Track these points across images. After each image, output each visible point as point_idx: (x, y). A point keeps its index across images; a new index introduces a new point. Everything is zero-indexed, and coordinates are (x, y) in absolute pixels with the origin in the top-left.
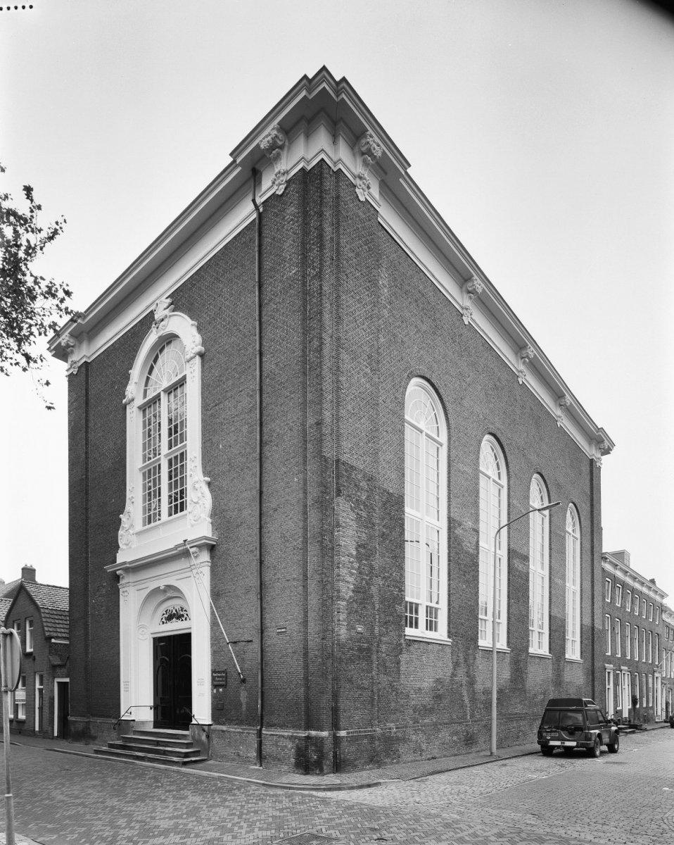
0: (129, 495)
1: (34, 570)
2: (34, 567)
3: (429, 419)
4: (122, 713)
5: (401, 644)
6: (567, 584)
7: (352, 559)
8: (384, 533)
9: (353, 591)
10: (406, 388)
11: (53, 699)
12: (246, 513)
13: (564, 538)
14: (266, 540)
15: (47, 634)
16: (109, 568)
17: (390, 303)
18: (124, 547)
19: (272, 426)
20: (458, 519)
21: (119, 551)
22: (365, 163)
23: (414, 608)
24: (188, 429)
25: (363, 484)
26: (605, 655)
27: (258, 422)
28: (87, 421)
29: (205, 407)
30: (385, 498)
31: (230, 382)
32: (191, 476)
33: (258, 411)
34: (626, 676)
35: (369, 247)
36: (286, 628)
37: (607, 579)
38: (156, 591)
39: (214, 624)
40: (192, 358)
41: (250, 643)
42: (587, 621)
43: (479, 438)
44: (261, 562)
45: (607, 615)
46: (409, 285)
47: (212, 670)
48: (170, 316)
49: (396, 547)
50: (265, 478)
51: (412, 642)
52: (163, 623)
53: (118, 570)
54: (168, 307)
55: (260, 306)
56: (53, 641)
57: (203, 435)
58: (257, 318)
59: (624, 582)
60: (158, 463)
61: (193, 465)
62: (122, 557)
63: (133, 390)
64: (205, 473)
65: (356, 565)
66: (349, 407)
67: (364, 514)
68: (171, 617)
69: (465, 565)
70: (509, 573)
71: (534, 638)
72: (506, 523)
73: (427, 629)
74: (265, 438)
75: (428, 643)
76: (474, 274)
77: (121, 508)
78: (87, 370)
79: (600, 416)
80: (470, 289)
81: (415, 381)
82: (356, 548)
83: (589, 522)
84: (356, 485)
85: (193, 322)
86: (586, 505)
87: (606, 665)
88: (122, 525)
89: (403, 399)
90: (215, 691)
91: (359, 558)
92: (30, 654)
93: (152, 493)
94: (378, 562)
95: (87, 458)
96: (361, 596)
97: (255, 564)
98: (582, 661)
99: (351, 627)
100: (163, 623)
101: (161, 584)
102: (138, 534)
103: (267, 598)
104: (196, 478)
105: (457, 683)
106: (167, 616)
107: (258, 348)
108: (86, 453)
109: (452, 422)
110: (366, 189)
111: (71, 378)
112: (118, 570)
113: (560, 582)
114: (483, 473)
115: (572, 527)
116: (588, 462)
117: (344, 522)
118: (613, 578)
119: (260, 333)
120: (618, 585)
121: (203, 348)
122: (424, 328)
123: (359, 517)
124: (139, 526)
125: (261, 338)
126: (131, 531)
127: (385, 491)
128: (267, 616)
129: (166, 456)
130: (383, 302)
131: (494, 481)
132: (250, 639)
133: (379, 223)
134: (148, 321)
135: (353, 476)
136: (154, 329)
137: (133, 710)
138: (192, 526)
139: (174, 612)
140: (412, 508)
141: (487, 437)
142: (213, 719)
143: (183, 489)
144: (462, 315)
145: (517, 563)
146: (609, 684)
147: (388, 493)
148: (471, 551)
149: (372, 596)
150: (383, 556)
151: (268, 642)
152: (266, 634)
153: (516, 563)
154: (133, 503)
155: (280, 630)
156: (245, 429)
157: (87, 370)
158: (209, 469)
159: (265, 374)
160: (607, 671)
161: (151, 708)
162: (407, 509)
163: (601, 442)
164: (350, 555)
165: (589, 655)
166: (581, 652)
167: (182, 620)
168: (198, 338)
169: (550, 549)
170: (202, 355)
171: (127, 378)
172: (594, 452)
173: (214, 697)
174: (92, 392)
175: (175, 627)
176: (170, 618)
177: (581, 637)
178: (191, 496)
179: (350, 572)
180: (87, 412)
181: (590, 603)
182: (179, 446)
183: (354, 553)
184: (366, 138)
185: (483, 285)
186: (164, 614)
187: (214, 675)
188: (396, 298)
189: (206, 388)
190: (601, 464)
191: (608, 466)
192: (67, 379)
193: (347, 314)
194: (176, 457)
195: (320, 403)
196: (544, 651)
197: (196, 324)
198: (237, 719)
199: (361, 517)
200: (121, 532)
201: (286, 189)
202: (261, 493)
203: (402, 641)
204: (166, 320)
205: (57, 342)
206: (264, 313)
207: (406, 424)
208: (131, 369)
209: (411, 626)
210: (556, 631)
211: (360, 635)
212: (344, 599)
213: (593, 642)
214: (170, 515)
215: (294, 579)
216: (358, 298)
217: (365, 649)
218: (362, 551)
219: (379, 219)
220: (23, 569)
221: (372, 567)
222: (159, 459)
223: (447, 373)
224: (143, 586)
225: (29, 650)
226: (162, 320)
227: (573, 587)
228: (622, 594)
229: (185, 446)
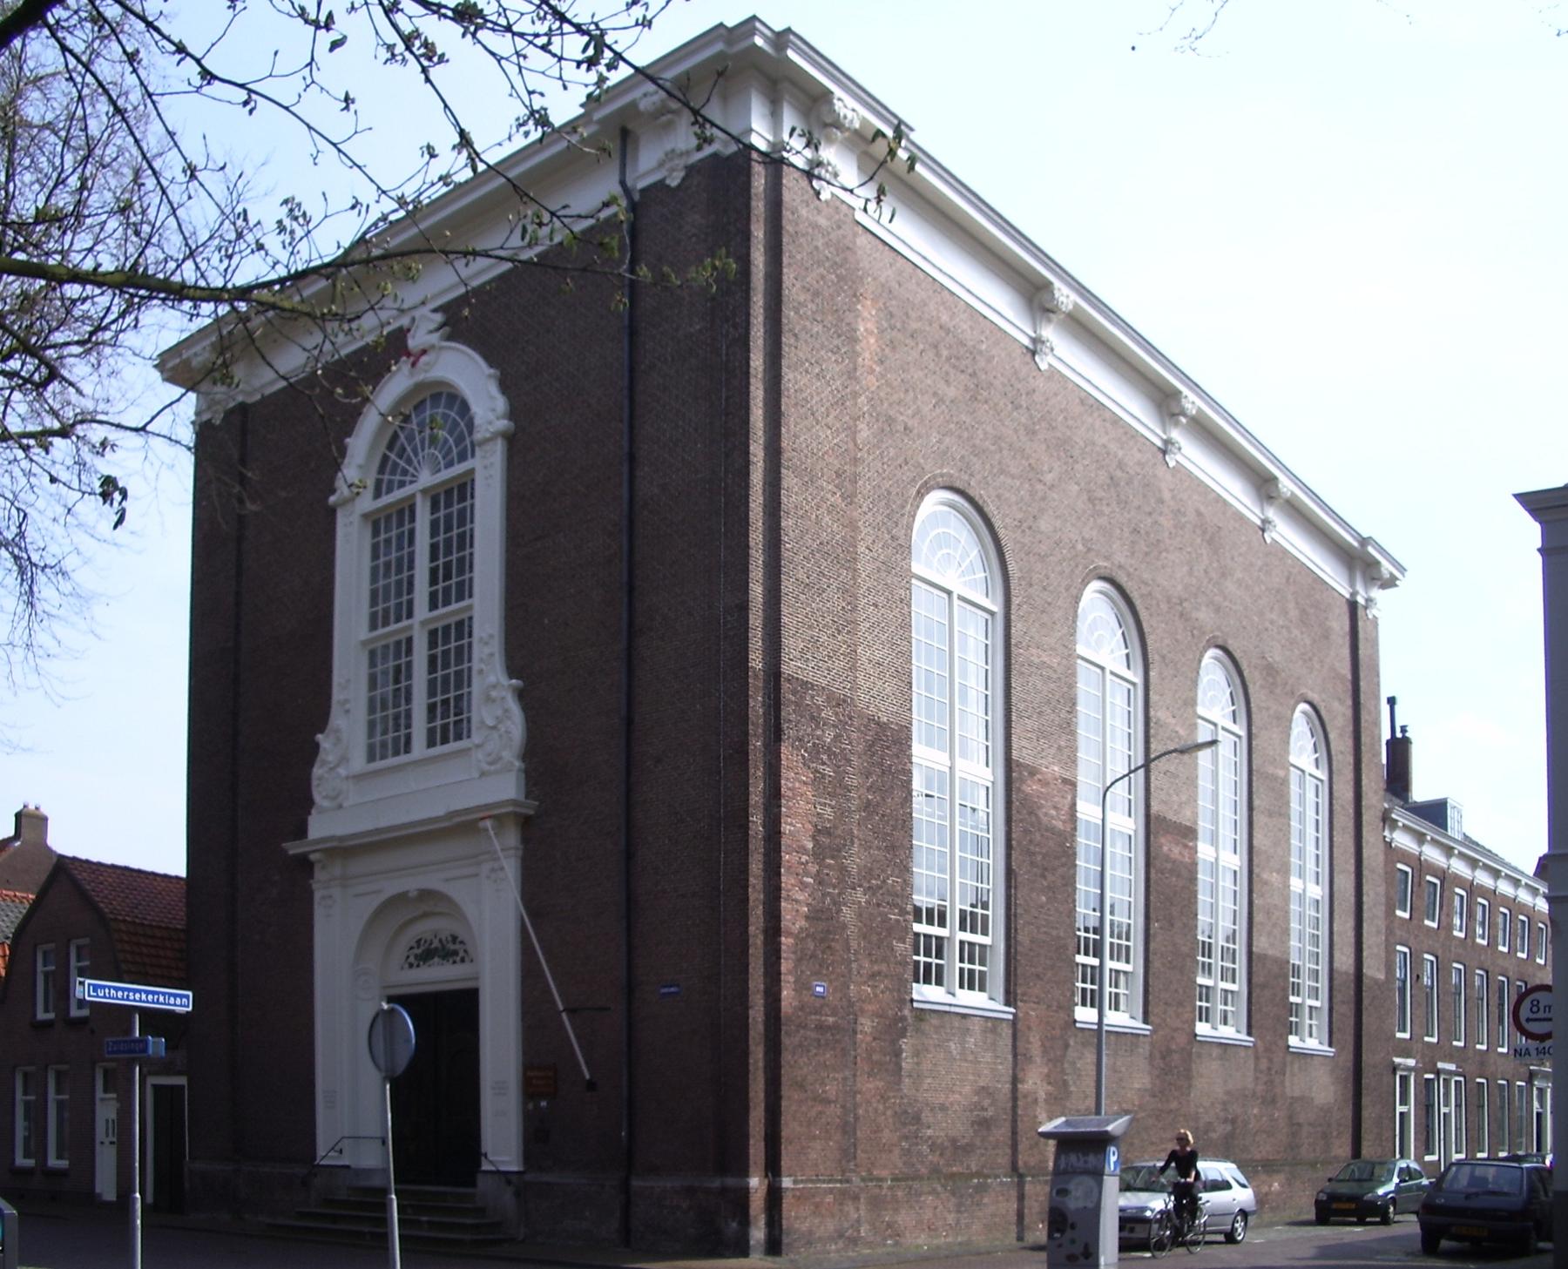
0: (337, 695)
2: (44, 810)
3: (964, 565)
4: (321, 1152)
5: (903, 1019)
7: (804, 858)
8: (869, 802)
9: (807, 918)
10: (914, 517)
13: (1285, 782)
16: (294, 848)
18: (326, 803)
21: (313, 811)
24: (477, 574)
36: (678, 986)
37: (1400, 866)
38: (400, 900)
42: (1345, 961)
43: (1074, 592)
46: (920, 319)
51: (921, 1015)
53: (314, 851)
61: (487, 650)
62: (320, 827)
64: (512, 671)
65: (813, 868)
66: (801, 575)
67: (828, 771)
68: (427, 953)
69: (1045, 856)
73: (961, 986)
75: (964, 1016)
77: (320, 718)
82: (814, 838)
83: (1350, 742)
85: (492, 371)
87: (1397, 1060)
88: (322, 756)
89: (909, 537)
90: (531, 1106)
94: (855, 859)
99: (803, 986)
100: (411, 966)
102: (359, 778)
104: (492, 679)
106: (418, 951)
111: (204, 431)
112: (314, 851)
113: (1274, 878)
117: (789, 789)
118: (1416, 864)
120: (1429, 878)
121: (512, 424)
122: (951, 392)
123: (819, 778)
124: (358, 762)
127: (871, 719)
129: (423, 623)
134: (395, 346)
137: (345, 1144)
138: (483, 774)
140: (929, 743)
145: (1168, 847)
146: (1404, 1101)
147: (878, 724)
148: (1060, 825)
150: (866, 846)
154: (347, 711)
160: (1399, 1074)
167: (454, 962)
168: (501, 403)
175: (438, 976)
178: (481, 713)
183: (810, 845)
186: (412, 948)
187: (529, 1074)
188: (894, 349)
193: (796, 404)
194: (447, 628)
197: (498, 373)
199: (824, 776)
200: (317, 771)
201: (684, 179)
202: (629, 722)
203: (906, 1012)
208: (349, 434)
210: (1264, 986)
211: (822, 1001)
212: (789, 934)
216: (817, 371)
217: (829, 1027)
218: (825, 840)
220: (18, 816)
221: (843, 869)
223: (1002, 472)
226: (424, 352)
229: (470, 607)
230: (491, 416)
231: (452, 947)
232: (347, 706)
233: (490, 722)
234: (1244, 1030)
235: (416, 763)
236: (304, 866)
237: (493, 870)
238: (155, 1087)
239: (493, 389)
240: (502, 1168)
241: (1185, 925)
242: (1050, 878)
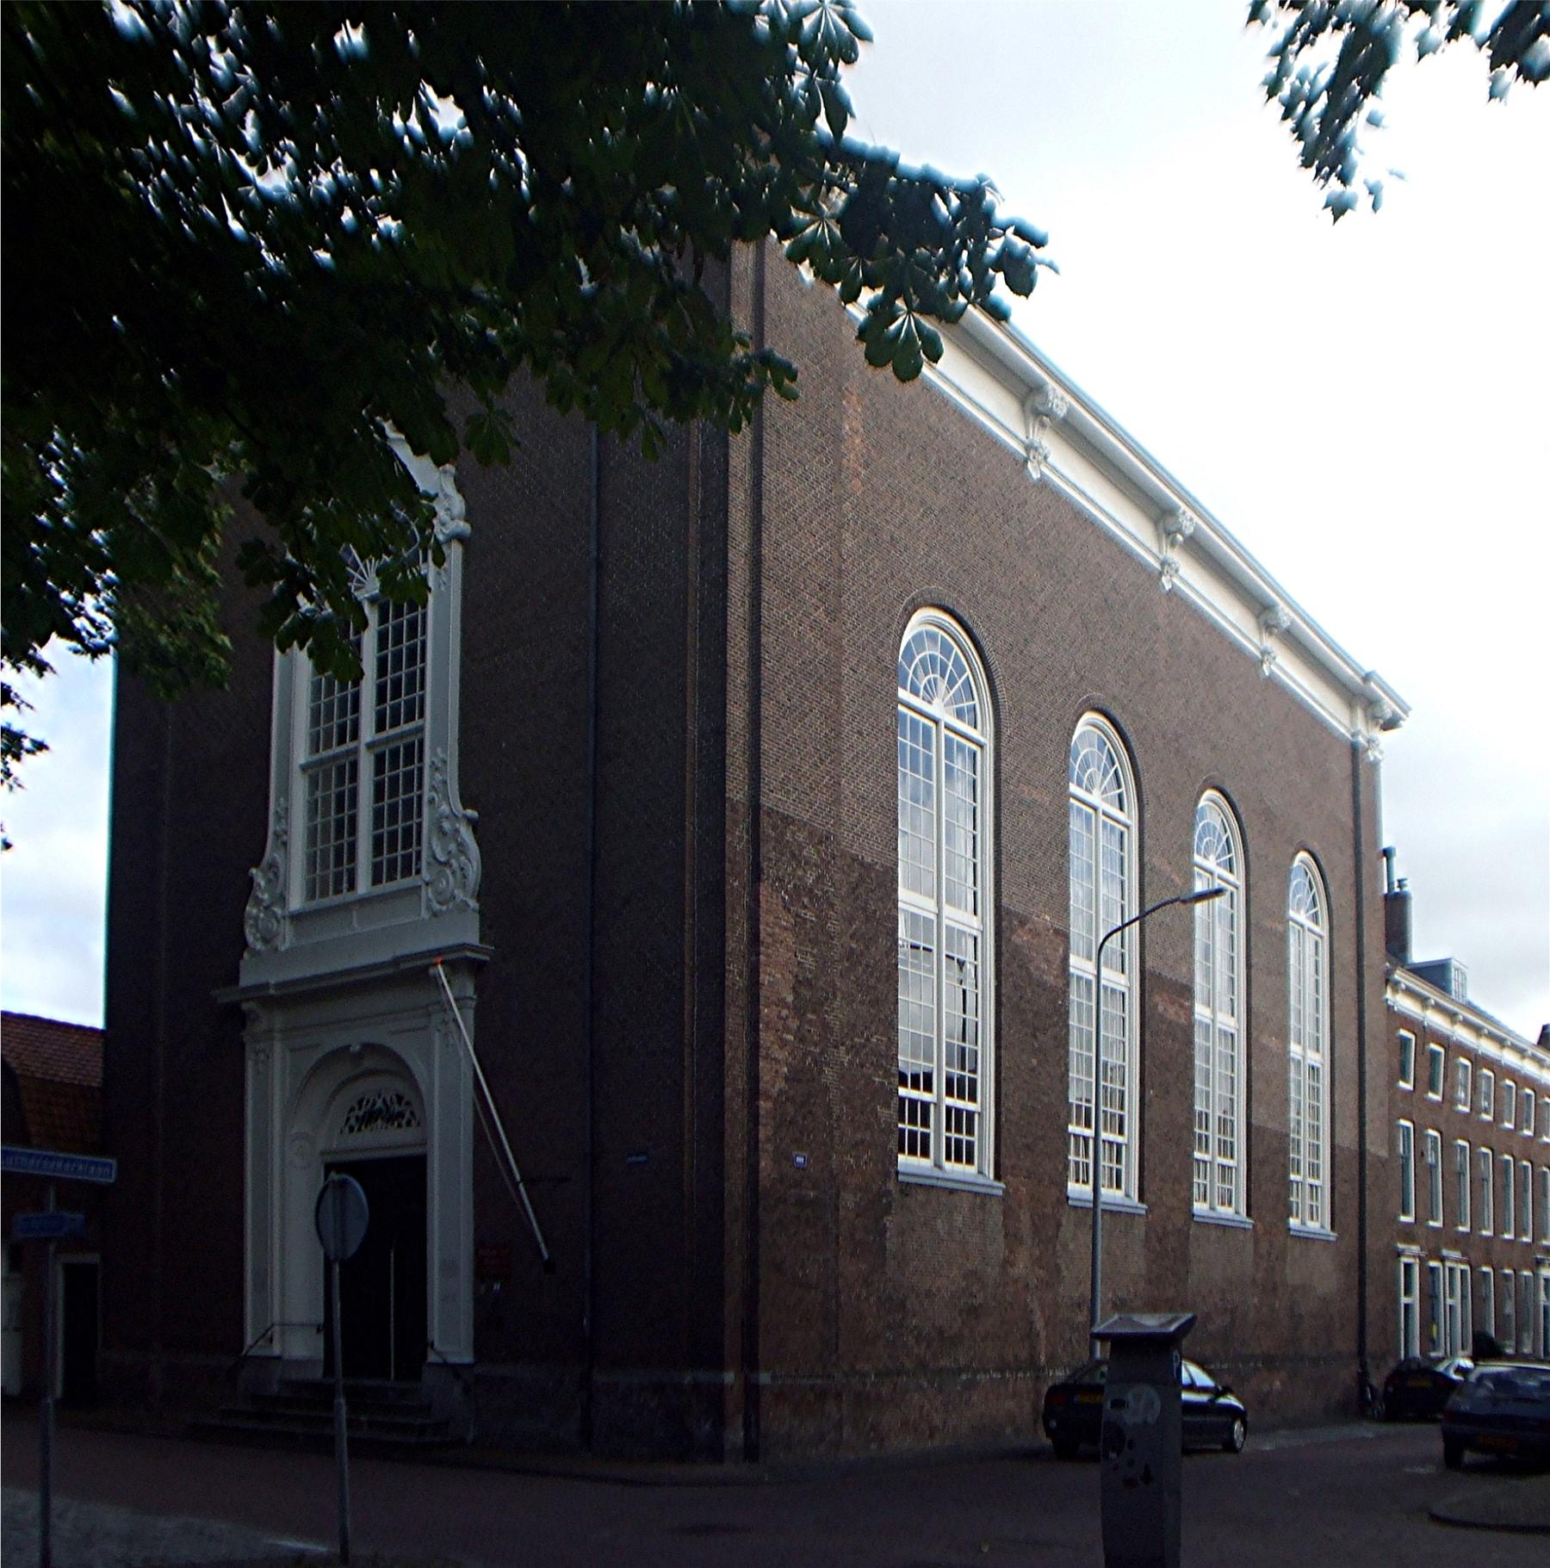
4: (249, 1340)
9: (787, 1079)
13: (1283, 939)
16: (224, 996)
17: (867, 465)
20: (1019, 909)
25: (809, 852)
30: (856, 875)
35: (822, 367)
38: (341, 1053)
39: (482, 1138)
42: (1348, 1138)
52: (351, 1129)
59: (1448, 1038)
60: (351, 758)
65: (794, 1024)
66: (782, 697)
67: (810, 916)
72: (1135, 913)
84: (793, 855)
86: (1341, 852)
87: (1401, 1246)
90: (483, 1289)
91: (799, 1010)
93: (332, 835)
94: (838, 1014)
98: (1333, 1236)
101: (354, 1039)
102: (296, 918)
105: (1016, 1281)
106: (361, 1113)
109: (1002, 695)
116: (1347, 752)
127: (854, 859)
129: (370, 746)
130: (852, 464)
135: (788, 837)
138: (435, 915)
139: (379, 1104)
145: (1163, 1006)
146: (1408, 1292)
147: (862, 864)
149: (827, 1089)
153: (1161, 1004)
161: (319, 1331)
162: (903, 893)
164: (782, 1003)
167: (400, 1126)
169: (1249, 966)
172: (1360, 725)
173: (479, 1301)
176: (369, 1118)
178: (432, 846)
179: (833, 614)
181: (1354, 1094)
182: (405, 727)
183: (790, 999)
196: (1233, 1211)
199: (805, 920)
209: (913, 1152)
210: (1263, 1163)
214: (376, 880)
218: (805, 992)
221: (825, 1025)
231: (397, 1108)
236: (236, 1017)
240: (453, 1359)
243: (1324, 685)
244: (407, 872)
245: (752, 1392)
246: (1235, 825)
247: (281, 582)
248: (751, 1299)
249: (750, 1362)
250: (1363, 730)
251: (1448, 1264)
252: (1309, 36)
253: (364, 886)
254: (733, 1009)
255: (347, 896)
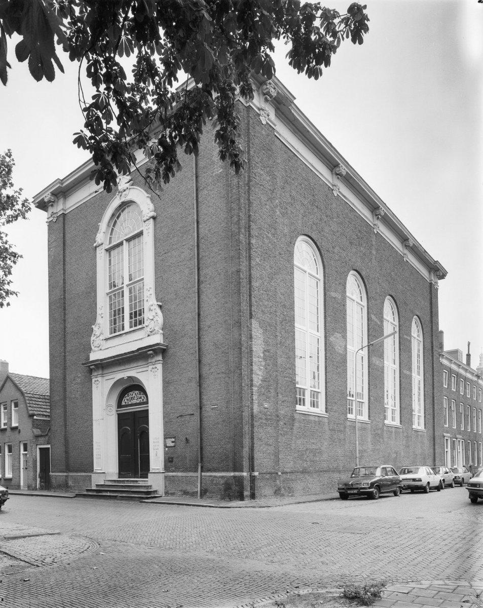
1: (7, 364)
6: (413, 374)
9: (262, 380)
11: (36, 460)
12: (188, 327)
13: (410, 341)
14: (202, 346)
15: (31, 412)
18: (96, 349)
19: (206, 271)
22: (266, 100)
23: (303, 391)
26: (443, 427)
27: (196, 268)
28: (64, 256)
29: (157, 254)
31: (176, 239)
32: (147, 301)
33: (196, 260)
34: (461, 442)
40: (148, 220)
41: (192, 416)
44: (200, 362)
45: (445, 397)
47: (165, 435)
48: (130, 189)
49: (289, 350)
50: (202, 305)
54: (128, 182)
55: (197, 190)
56: (35, 417)
57: (156, 273)
58: (195, 198)
60: (122, 290)
63: (100, 237)
70: (369, 367)
71: (415, 420)
73: (311, 406)
74: (202, 279)
76: (340, 162)
77: (93, 320)
78: (64, 219)
79: (435, 253)
80: (337, 172)
81: (301, 238)
85: (148, 195)
88: (94, 333)
92: (16, 428)
95: (64, 283)
96: (266, 383)
97: (196, 363)
99: (260, 405)
103: (204, 386)
104: (151, 303)
107: (196, 219)
108: (64, 279)
110: (267, 117)
111: (51, 225)
114: (348, 297)
115: (416, 333)
119: (197, 208)
120: (453, 375)
125: (197, 211)
126: (101, 338)
128: (204, 397)
129: (127, 286)
131: (357, 302)
132: (192, 413)
133: (275, 135)
136: (118, 197)
141: (352, 272)
142: (165, 469)
143: (141, 309)
144: (332, 190)
145: (375, 360)
146: (447, 448)
151: (205, 414)
152: (203, 409)
154: (102, 317)
155: (213, 407)
156: (187, 271)
157: (64, 219)
158: (160, 296)
159: (201, 236)
160: (446, 438)
163: (437, 271)
165: (430, 426)
166: (425, 424)
168: (152, 206)
170: (154, 218)
171: (97, 229)
174: (68, 236)
177: (425, 413)
178: (147, 315)
180: (64, 250)
183: (262, 355)
184: (267, 85)
185: (346, 169)
189: (156, 240)
190: (438, 286)
191: (442, 286)
192: (47, 224)
195: (239, 258)
197: (150, 196)
198: (183, 468)
200: (92, 338)
204: (127, 192)
205: (41, 198)
206: (200, 196)
207: (295, 267)
208: (100, 222)
213: (434, 417)
214: (131, 327)
215: (223, 373)
219: (275, 133)
222: (123, 287)
224: (110, 377)
225: (14, 424)
226: (125, 191)
227: (419, 377)
228: (457, 381)
230: (148, 211)
232: (102, 316)
233: (151, 318)
234: (399, 423)
235: (126, 333)
237: (153, 368)
238: (40, 449)
239: (149, 201)
241: (380, 387)
242: (339, 369)
243: (397, 240)
244: (140, 324)
245: (253, 479)
246: (395, 306)
247: (111, 184)
248: (252, 449)
249: (252, 468)
250: (433, 279)
251: (458, 439)
252: (337, 44)
253: (127, 329)
254: (244, 359)
255: (122, 332)
